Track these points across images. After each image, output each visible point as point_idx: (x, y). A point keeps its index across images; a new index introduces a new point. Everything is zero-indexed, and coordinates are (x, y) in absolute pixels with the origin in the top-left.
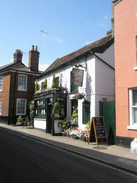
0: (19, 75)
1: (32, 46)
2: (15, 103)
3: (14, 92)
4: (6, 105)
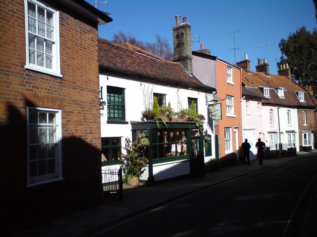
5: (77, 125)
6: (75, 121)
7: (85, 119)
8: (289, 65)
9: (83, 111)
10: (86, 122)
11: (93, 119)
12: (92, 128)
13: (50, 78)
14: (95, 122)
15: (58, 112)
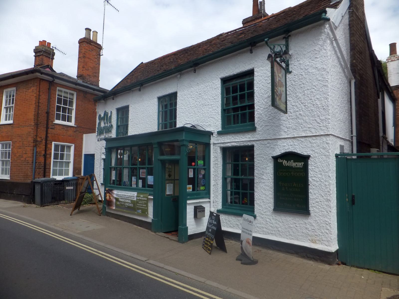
0: (58, 88)
1: (87, 29)
2: (48, 152)
3: (47, 128)
4: (25, 156)
5: (18, 149)
6: (17, 147)
7: (23, 145)
8: (262, 12)
9: (22, 140)
10: (23, 147)
11: (28, 144)
12: (27, 150)
13: (8, 126)
14: (29, 146)
15: (72, 145)
